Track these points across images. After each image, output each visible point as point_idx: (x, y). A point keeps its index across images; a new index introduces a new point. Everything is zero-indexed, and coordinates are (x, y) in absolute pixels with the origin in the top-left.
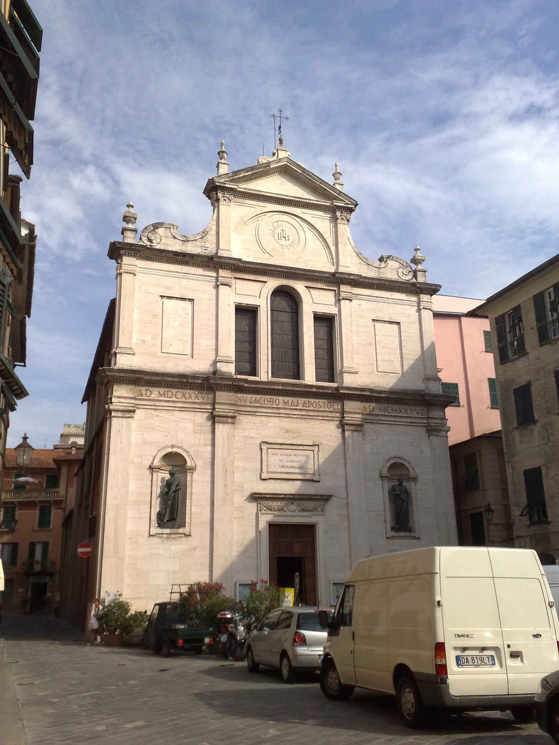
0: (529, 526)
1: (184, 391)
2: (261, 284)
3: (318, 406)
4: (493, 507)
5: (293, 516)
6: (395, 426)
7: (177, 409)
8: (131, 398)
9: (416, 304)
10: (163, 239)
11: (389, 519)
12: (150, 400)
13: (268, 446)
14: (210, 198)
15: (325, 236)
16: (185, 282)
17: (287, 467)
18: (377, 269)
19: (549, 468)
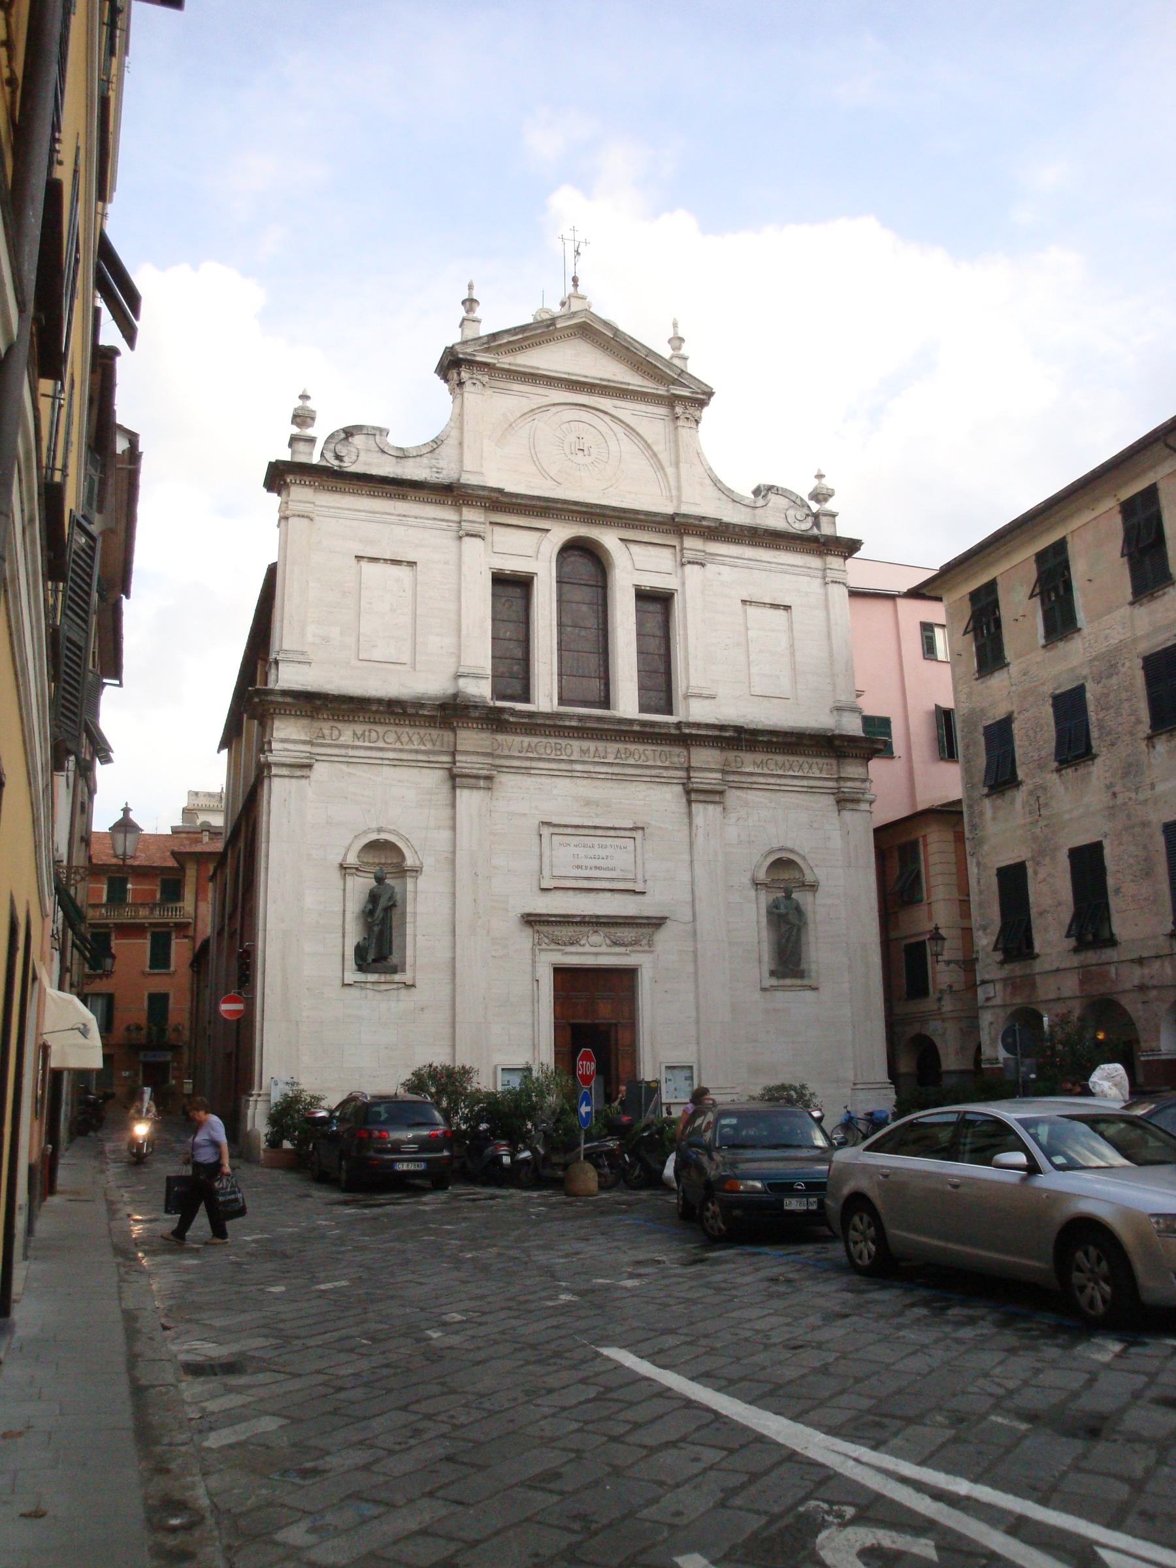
0: (1002, 963)
1: (400, 730)
2: (537, 534)
3: (643, 757)
4: (943, 932)
5: (597, 954)
6: (781, 794)
7: (387, 762)
8: (304, 742)
9: (820, 574)
10: (362, 454)
11: (766, 957)
12: (336, 746)
13: (552, 830)
14: (447, 381)
15: (655, 448)
16: (399, 531)
17: (586, 868)
18: (749, 510)
19: (1038, 863)
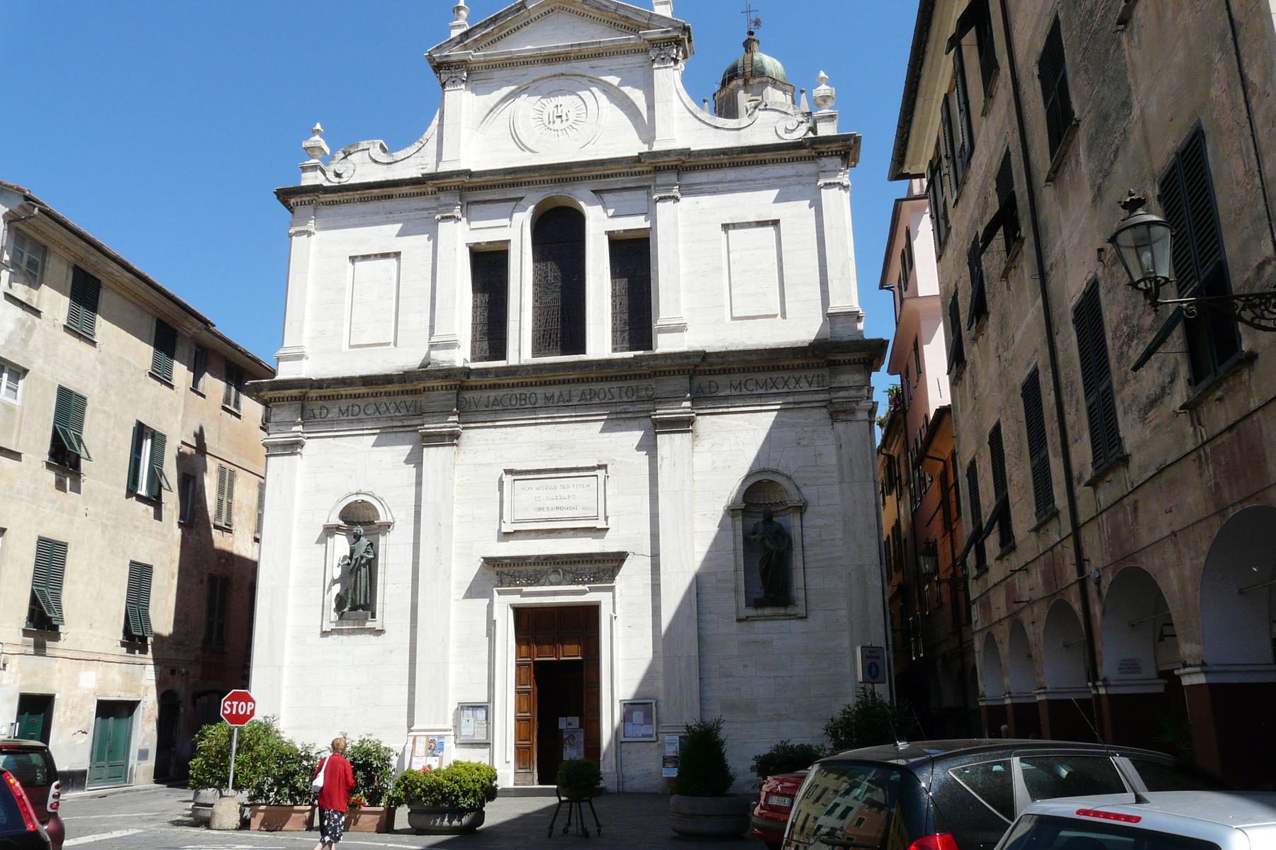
3: (609, 396)
